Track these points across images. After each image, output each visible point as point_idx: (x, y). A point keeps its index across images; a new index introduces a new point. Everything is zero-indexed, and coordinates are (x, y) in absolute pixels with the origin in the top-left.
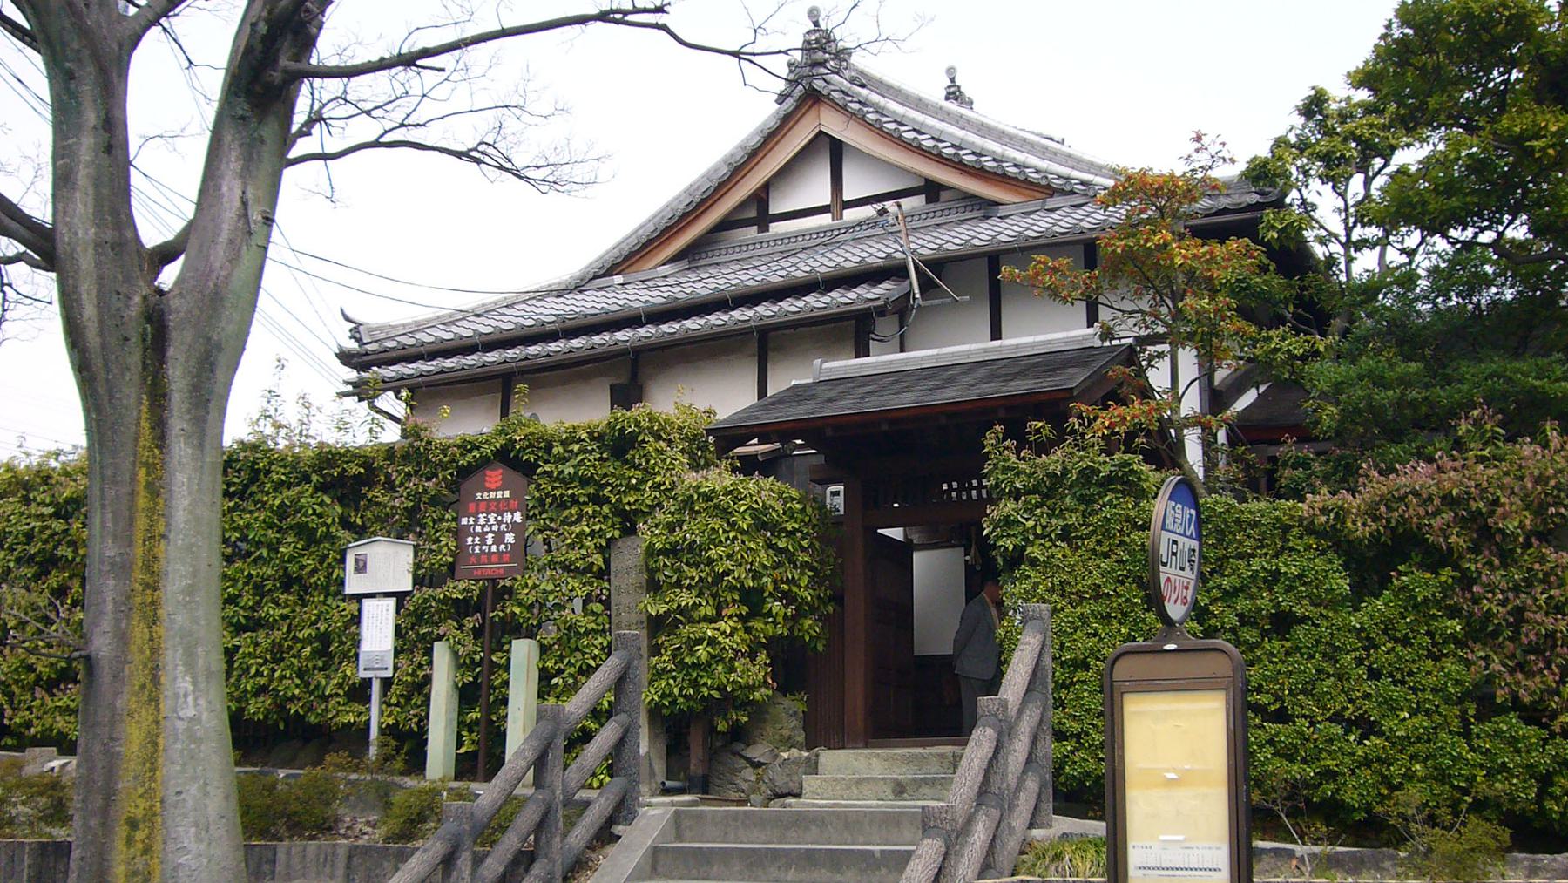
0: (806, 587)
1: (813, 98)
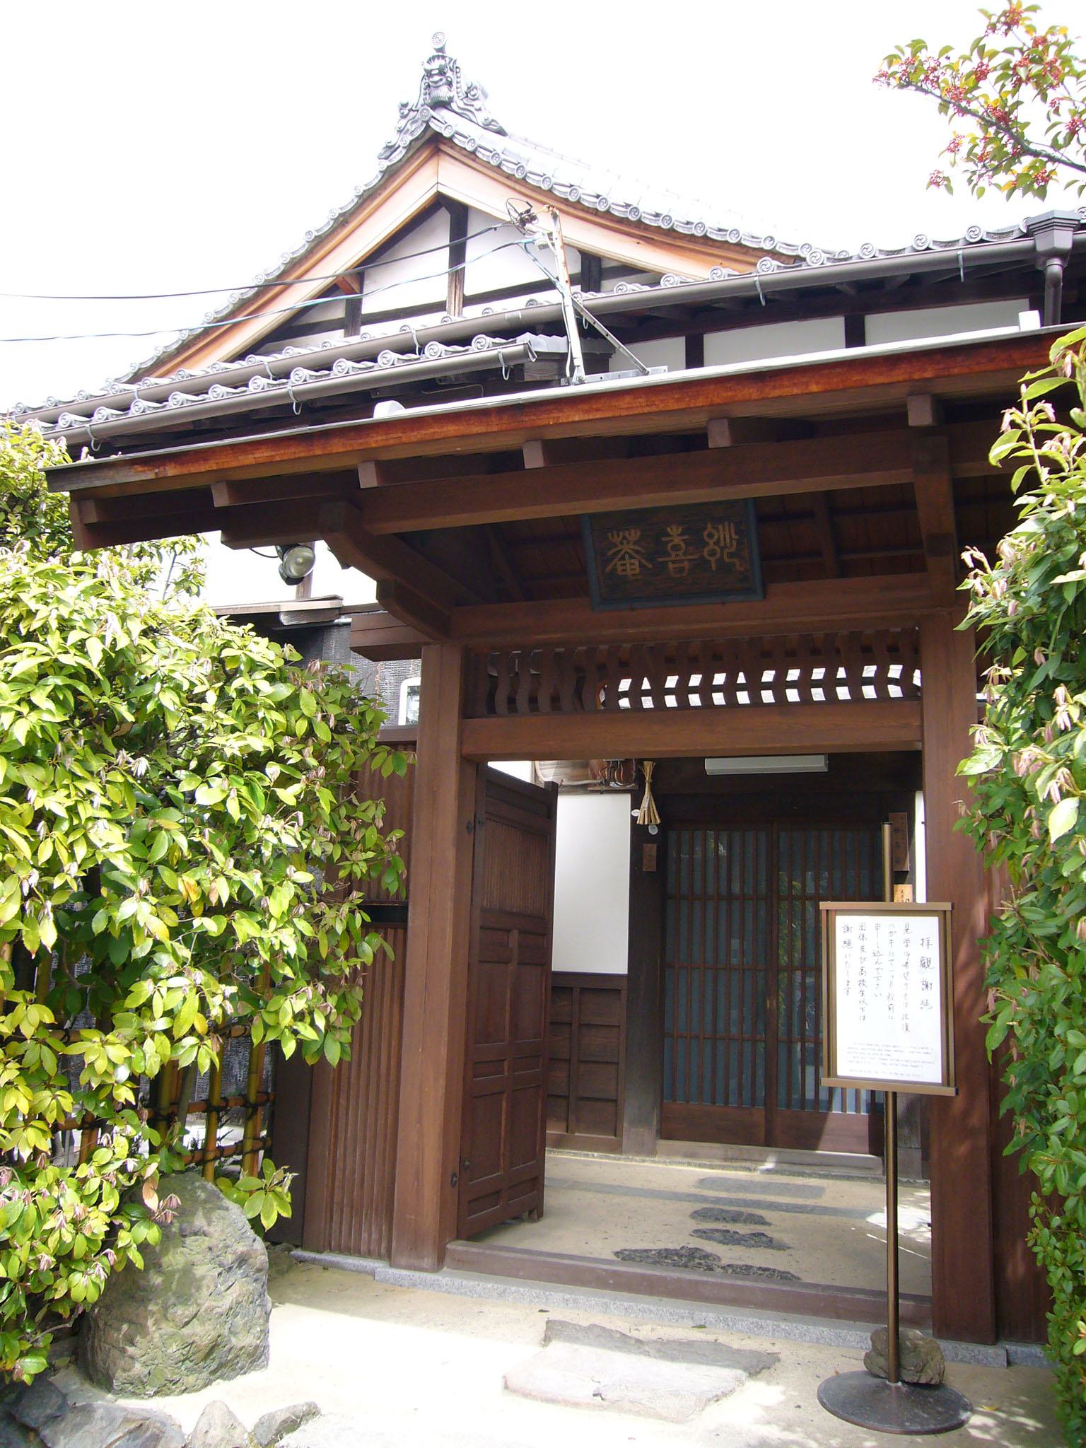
0: (288, 919)
1: (433, 144)
